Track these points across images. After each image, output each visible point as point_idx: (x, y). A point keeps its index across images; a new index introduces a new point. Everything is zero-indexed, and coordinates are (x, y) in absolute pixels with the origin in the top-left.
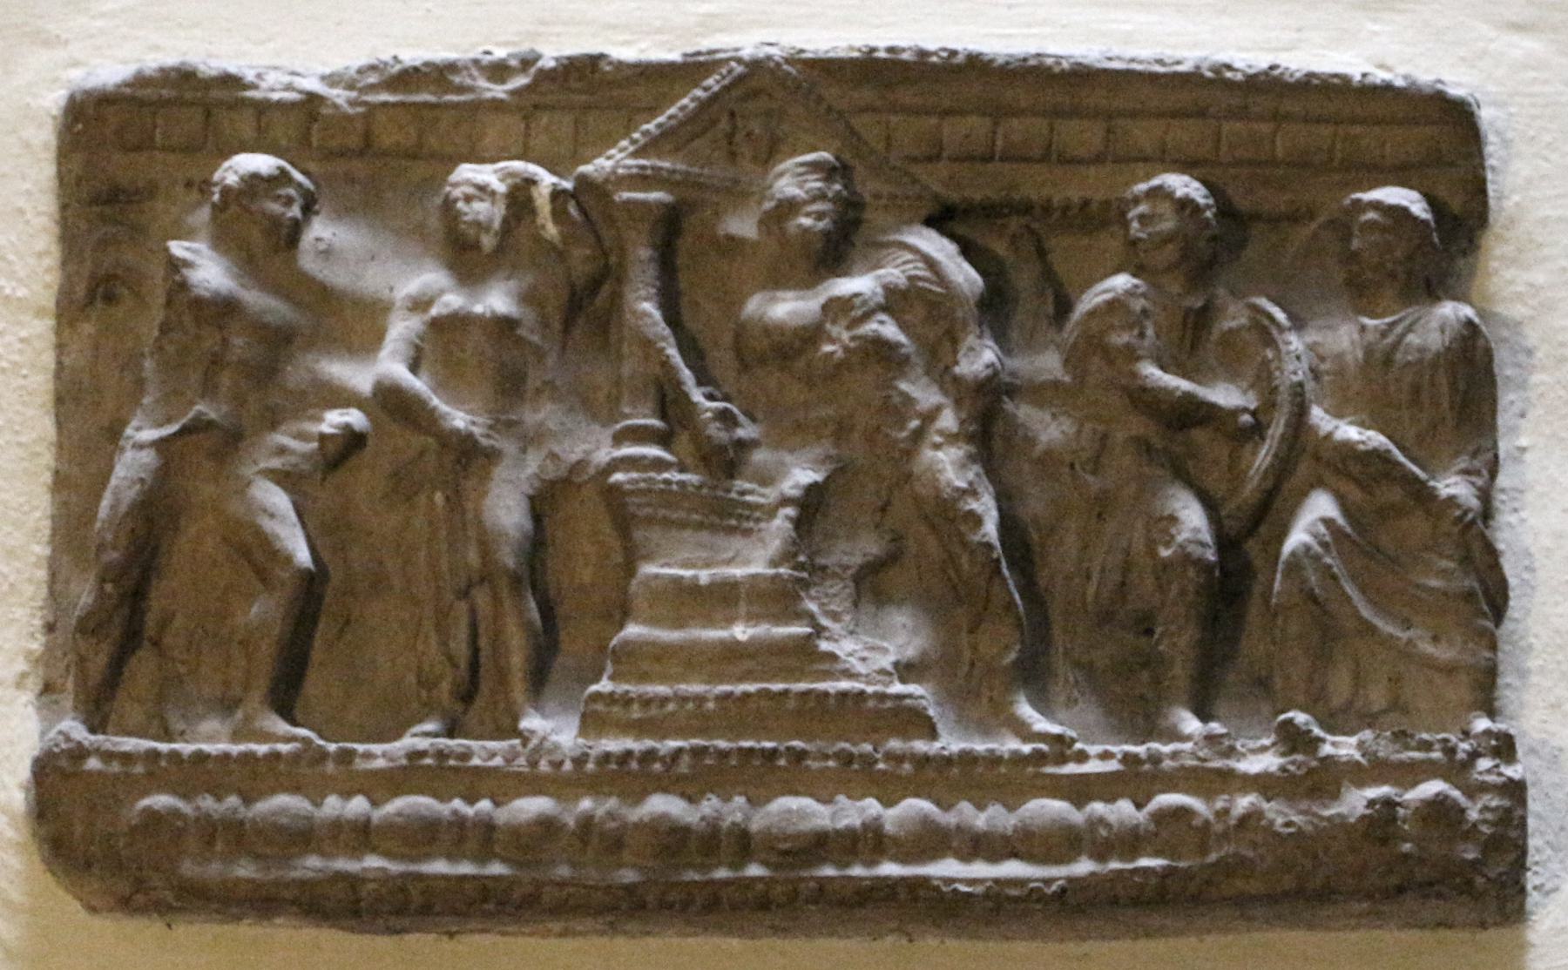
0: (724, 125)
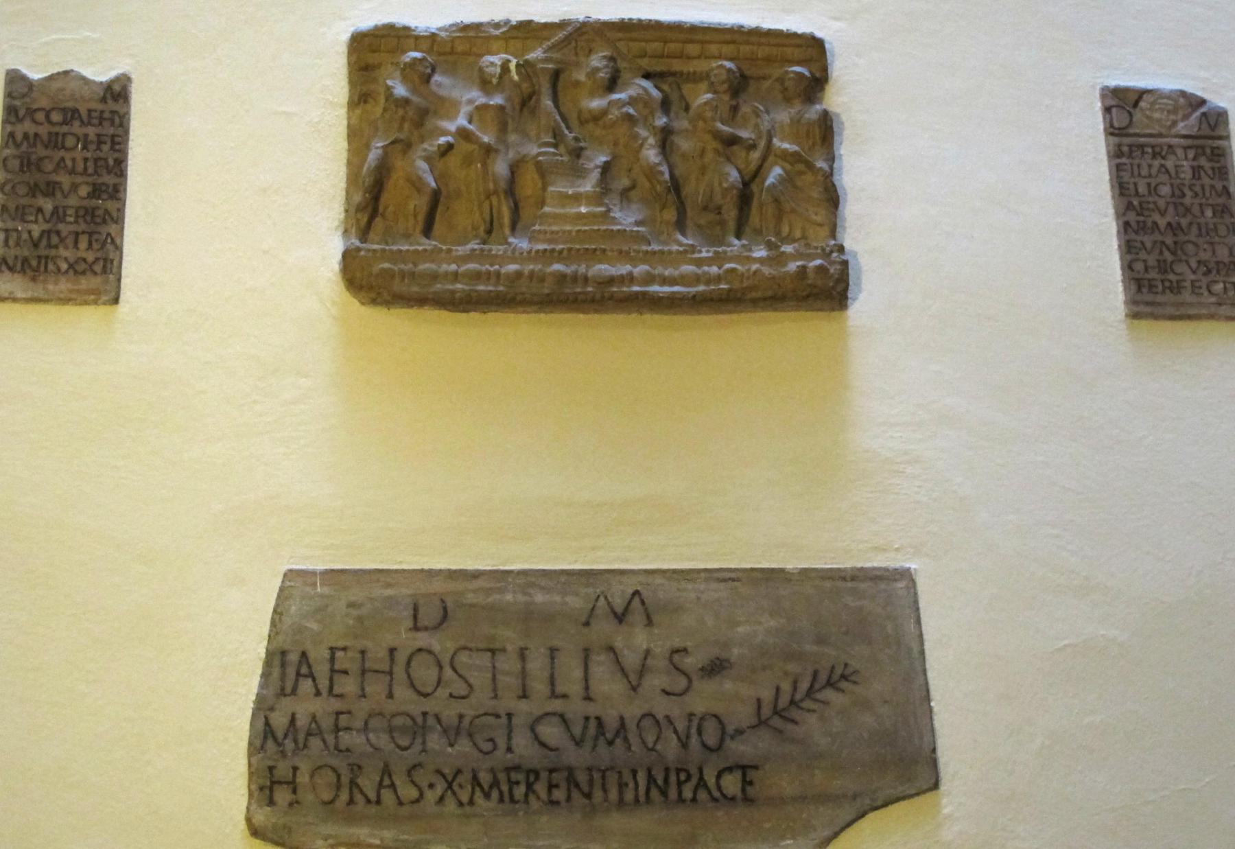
0: (573, 44)
